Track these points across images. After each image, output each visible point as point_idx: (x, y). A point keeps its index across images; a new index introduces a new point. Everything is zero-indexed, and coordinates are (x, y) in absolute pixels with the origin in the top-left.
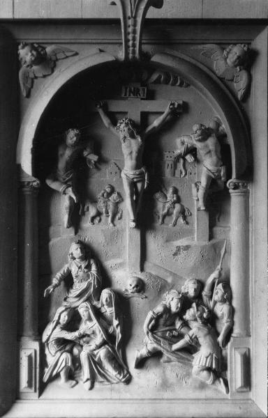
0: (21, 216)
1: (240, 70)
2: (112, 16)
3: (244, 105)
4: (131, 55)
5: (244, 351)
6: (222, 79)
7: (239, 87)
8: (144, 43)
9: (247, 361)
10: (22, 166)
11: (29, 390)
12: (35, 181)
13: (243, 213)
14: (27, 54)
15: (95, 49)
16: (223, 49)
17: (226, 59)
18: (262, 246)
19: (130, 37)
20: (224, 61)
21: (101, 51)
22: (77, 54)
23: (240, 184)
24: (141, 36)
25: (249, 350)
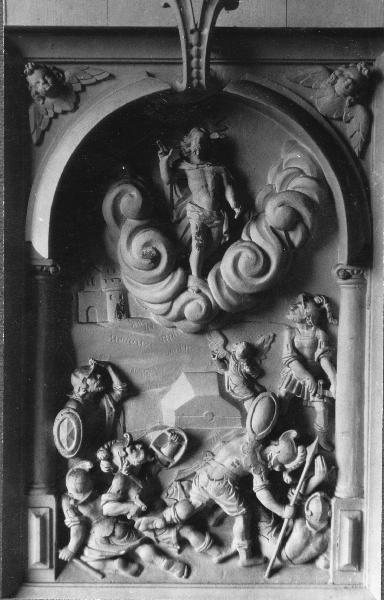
0: (31, 377)
2: (171, 24)
3: (363, 162)
4: (195, 82)
5: (356, 514)
6: (326, 118)
7: (353, 128)
11: (40, 566)
16: (331, 72)
17: (333, 84)
25: (362, 513)
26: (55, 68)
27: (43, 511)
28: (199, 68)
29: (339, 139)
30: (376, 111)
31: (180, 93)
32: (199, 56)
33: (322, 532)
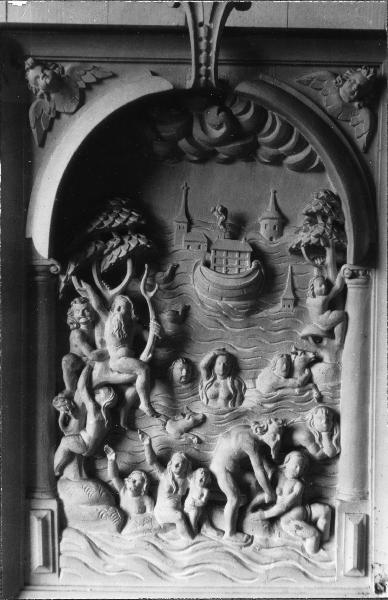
1: (360, 107)
3: (365, 156)
9: (363, 532)
10: (34, 240)
11: (45, 570)
12: (52, 265)
13: (360, 344)
18: (384, 402)
19: (203, 45)
20: (337, 90)
21: (154, 74)
23: (360, 272)
24: (217, 55)
25: (367, 517)
27: (44, 514)
29: (349, 146)
32: (207, 63)
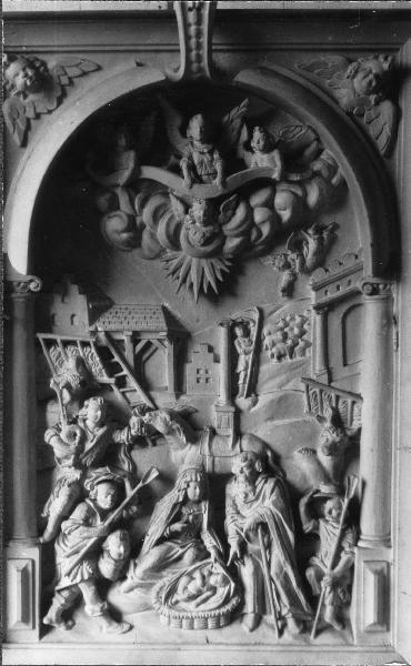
4: (195, 66)
8: (216, 51)
11: (23, 626)
14: (17, 75)
15: (129, 63)
21: (139, 65)
22: (99, 68)
23: (381, 287)
26: (37, 59)
28: (199, 46)
30: (403, 104)
31: (137, 151)
33: (186, 489)
